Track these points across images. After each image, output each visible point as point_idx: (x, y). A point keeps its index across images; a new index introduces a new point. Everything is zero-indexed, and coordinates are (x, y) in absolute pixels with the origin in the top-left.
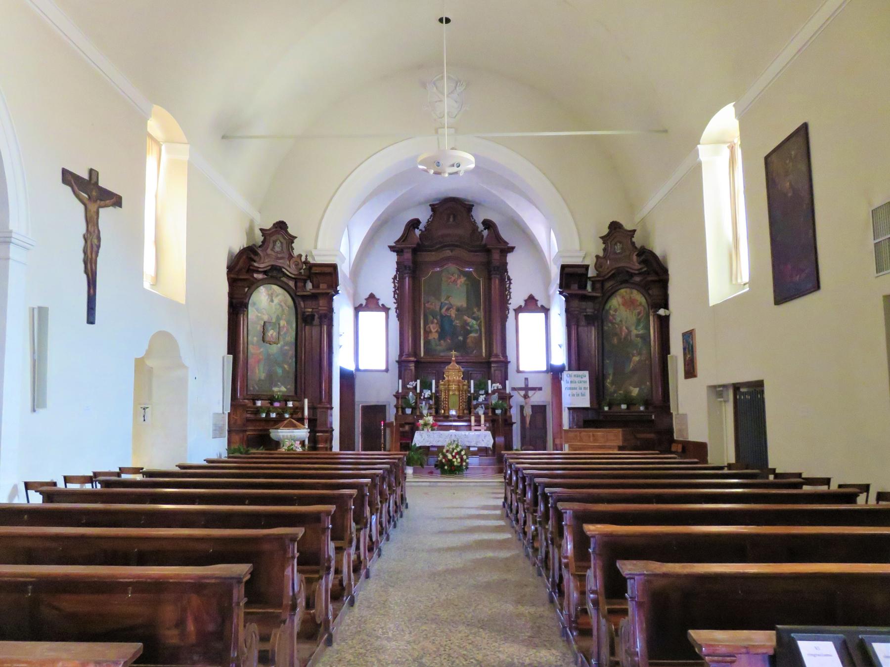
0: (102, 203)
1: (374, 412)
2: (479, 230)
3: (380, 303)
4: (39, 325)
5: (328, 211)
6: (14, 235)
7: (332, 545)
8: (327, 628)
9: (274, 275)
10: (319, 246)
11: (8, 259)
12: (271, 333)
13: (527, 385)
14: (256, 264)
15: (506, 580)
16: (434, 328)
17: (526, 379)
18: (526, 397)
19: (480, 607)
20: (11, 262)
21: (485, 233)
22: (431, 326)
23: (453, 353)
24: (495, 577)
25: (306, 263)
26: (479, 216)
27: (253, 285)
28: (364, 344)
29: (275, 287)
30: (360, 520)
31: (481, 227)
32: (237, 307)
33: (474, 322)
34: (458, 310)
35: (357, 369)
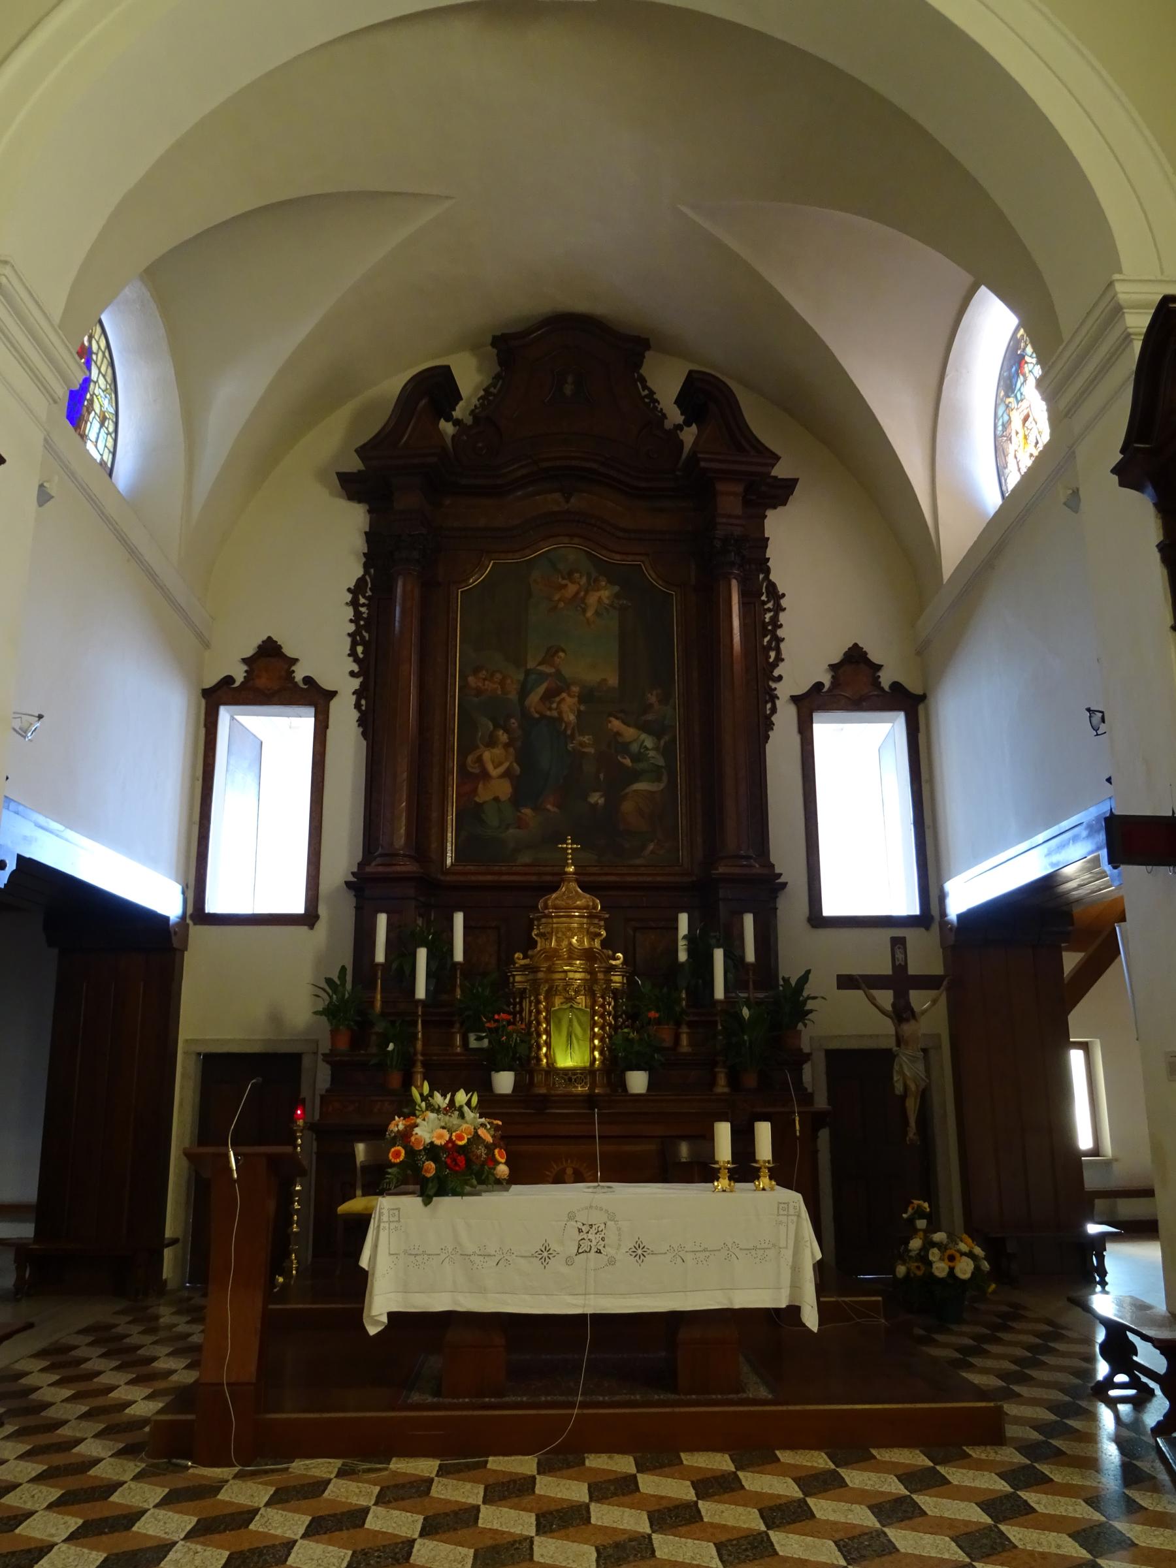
2: (668, 425)
3: (300, 673)
5: (379, 1249)
13: (900, 968)
16: (495, 760)
17: (898, 943)
18: (902, 1013)
22: (487, 756)
23: (569, 845)
33: (649, 742)
34: (588, 696)
35: (197, 912)
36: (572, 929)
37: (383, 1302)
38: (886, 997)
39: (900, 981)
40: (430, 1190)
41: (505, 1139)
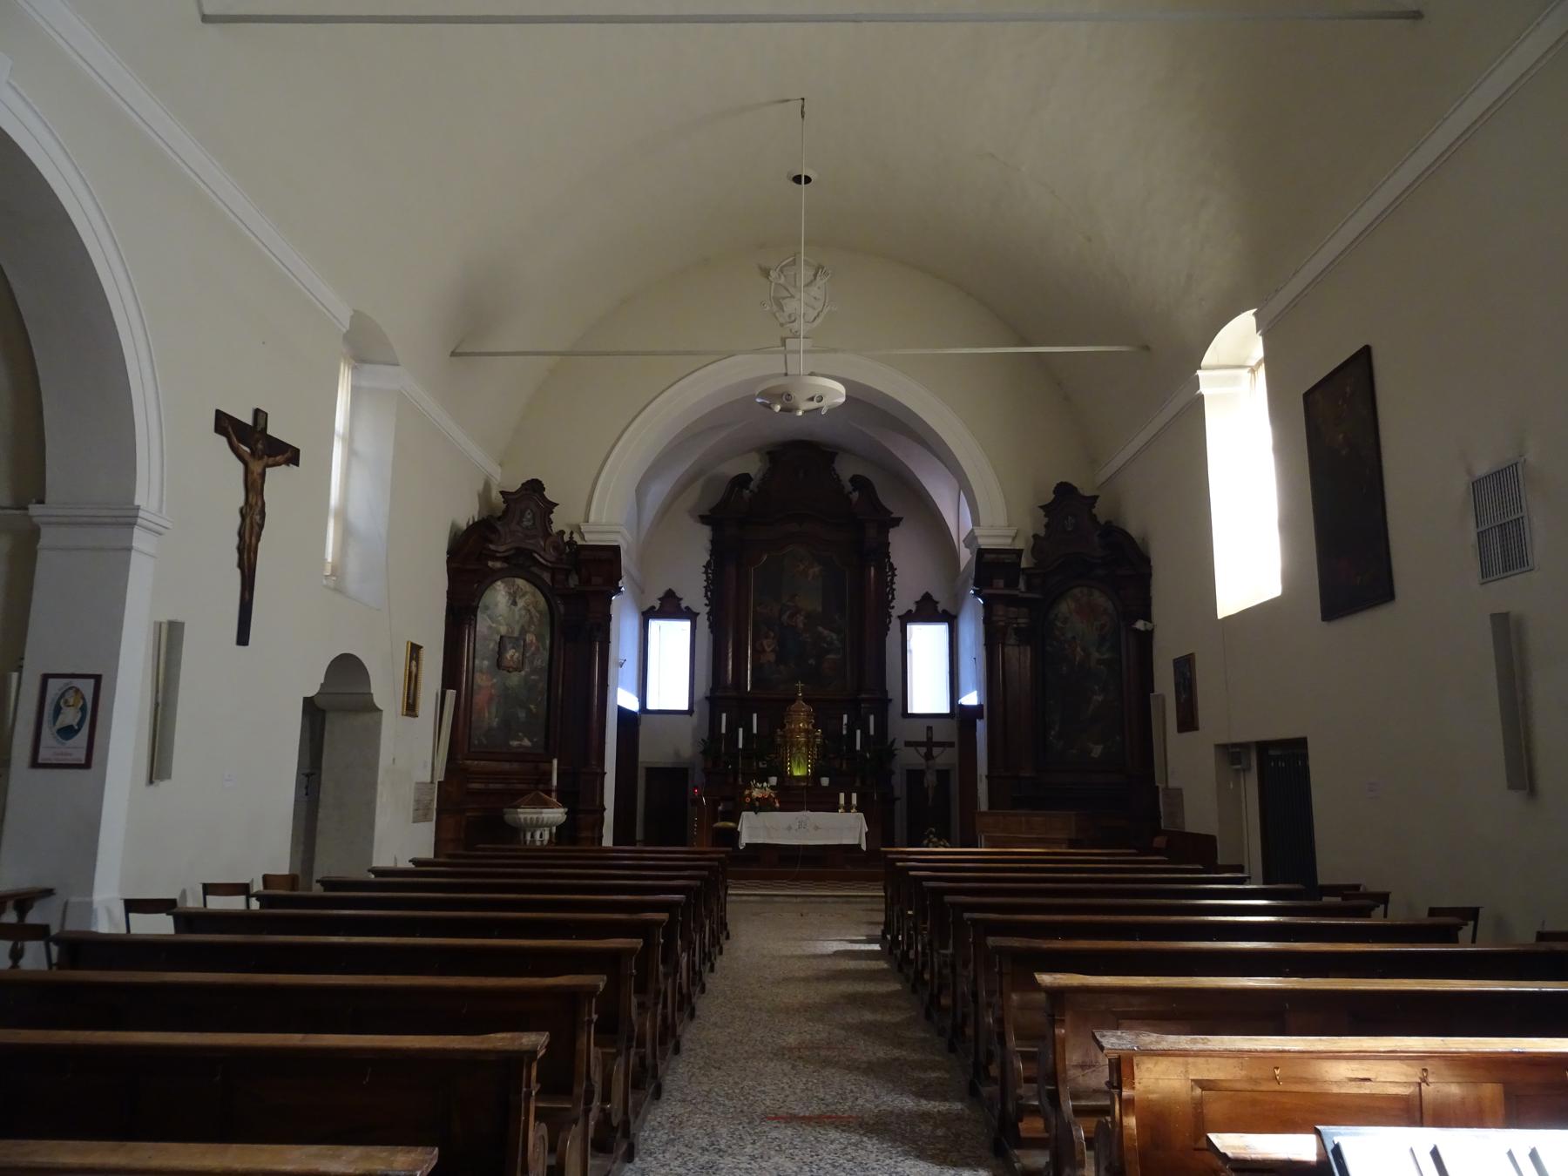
0: (271, 460)
1: (670, 778)
3: (683, 605)
4: (168, 652)
6: (141, 514)
7: (634, 1001)
8: (627, 1134)
9: (520, 564)
10: (592, 518)
11: (129, 549)
12: (511, 654)
13: (930, 739)
14: (492, 547)
15: (897, 1059)
16: (769, 645)
17: (930, 728)
18: (929, 756)
19: (860, 1102)
20: (133, 553)
21: (855, 495)
22: (765, 642)
23: (800, 685)
24: (881, 1054)
25: (571, 543)
26: (846, 470)
27: (487, 579)
28: (663, 668)
29: (520, 582)
30: (669, 956)
31: (848, 487)
32: (461, 611)
33: (834, 636)
36: (800, 721)
37: (745, 839)
38: (923, 750)
39: (930, 744)
40: (756, 810)
41: (777, 796)
